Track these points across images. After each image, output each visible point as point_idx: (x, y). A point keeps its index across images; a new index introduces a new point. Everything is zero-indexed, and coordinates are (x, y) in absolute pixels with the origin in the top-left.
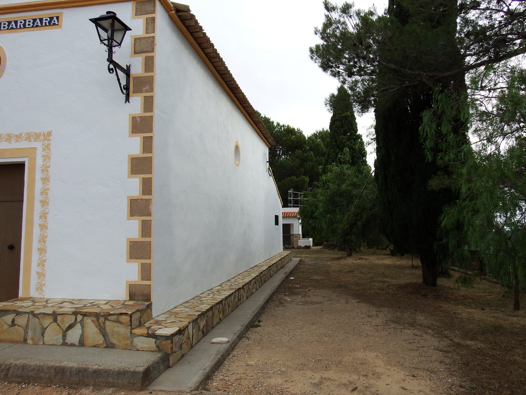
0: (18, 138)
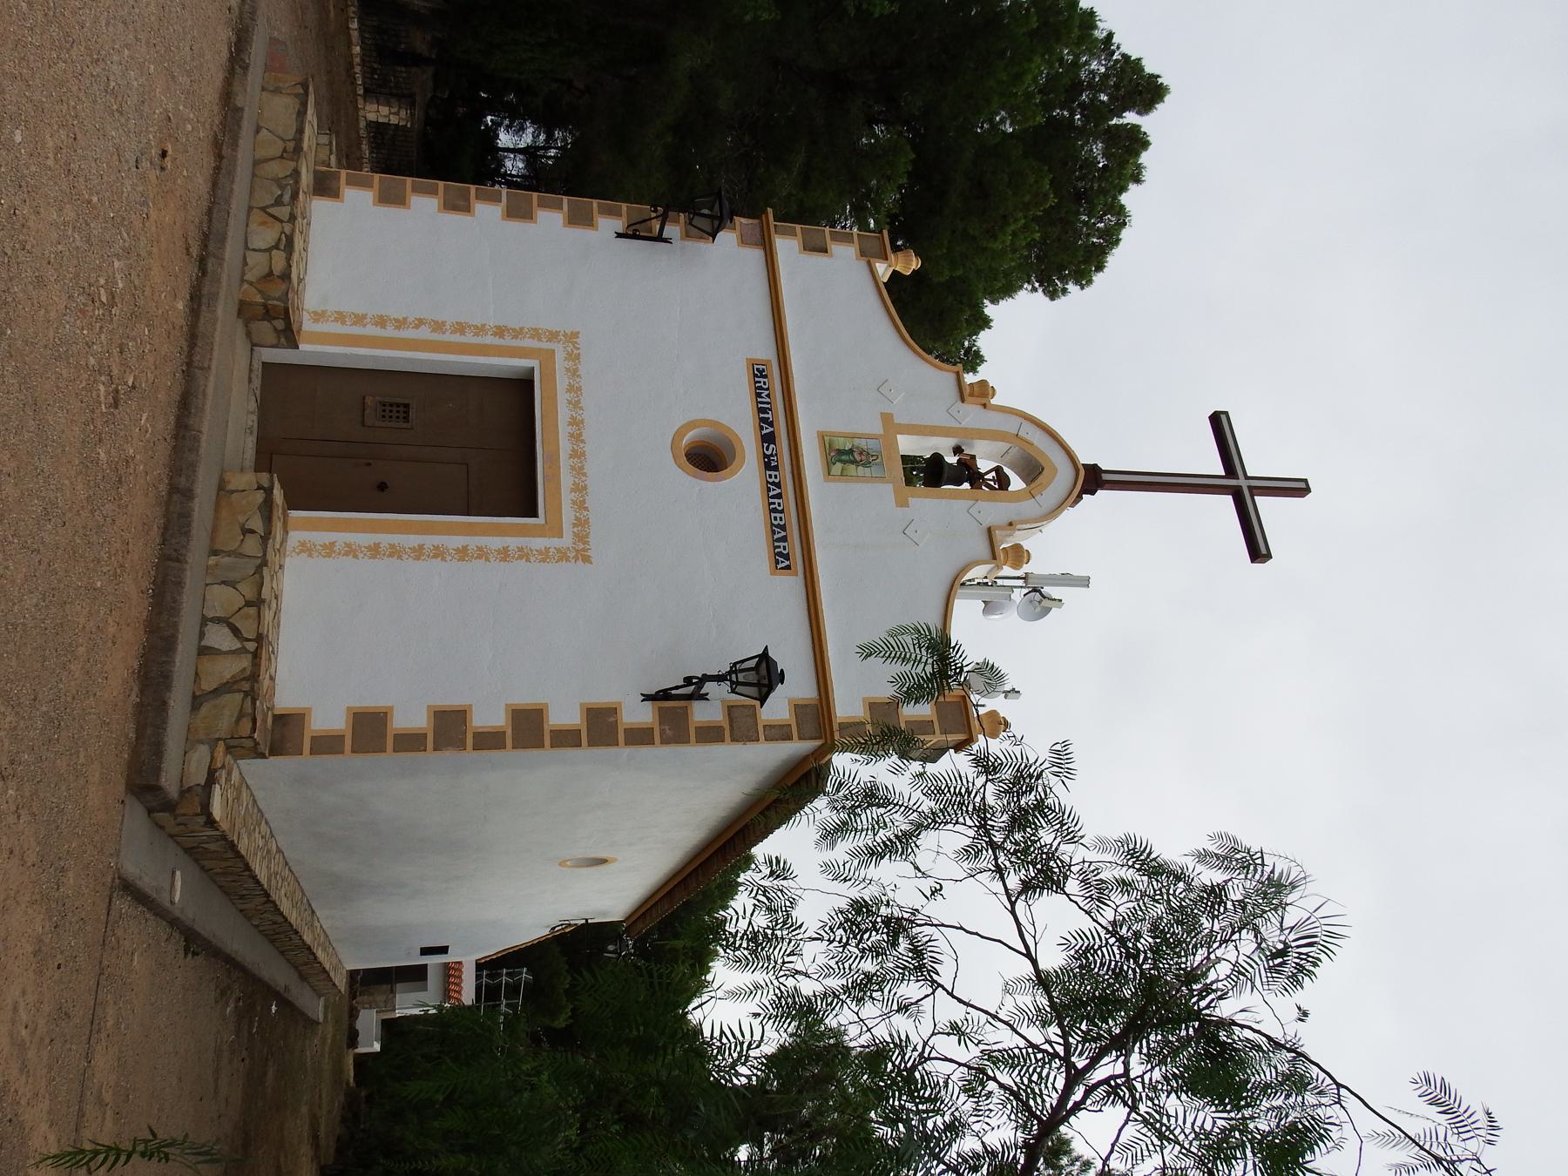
0: (581, 505)
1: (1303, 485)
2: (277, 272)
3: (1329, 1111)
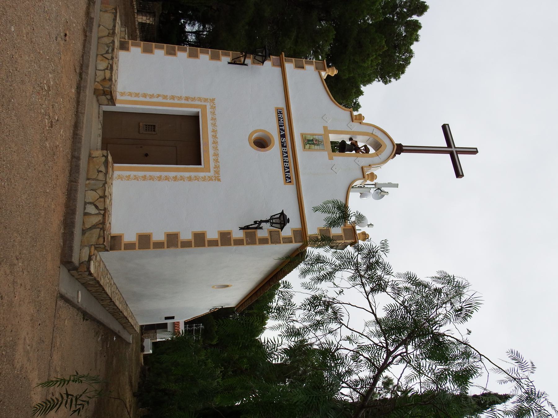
0: (216, 161)
1: (475, 150)
3: (478, 364)
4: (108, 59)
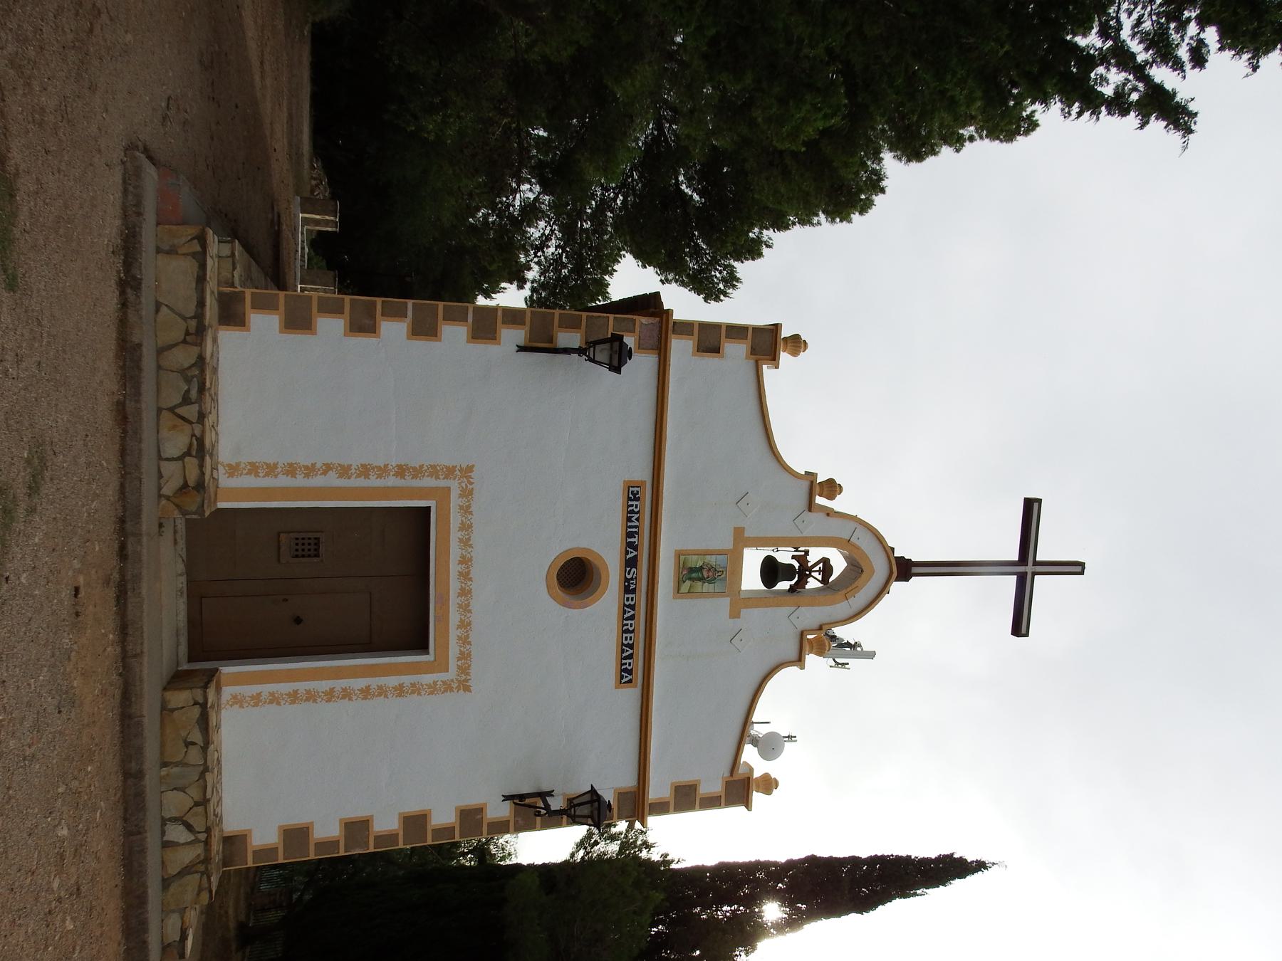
0: (464, 640)
2: (191, 483)
4: (191, 423)
